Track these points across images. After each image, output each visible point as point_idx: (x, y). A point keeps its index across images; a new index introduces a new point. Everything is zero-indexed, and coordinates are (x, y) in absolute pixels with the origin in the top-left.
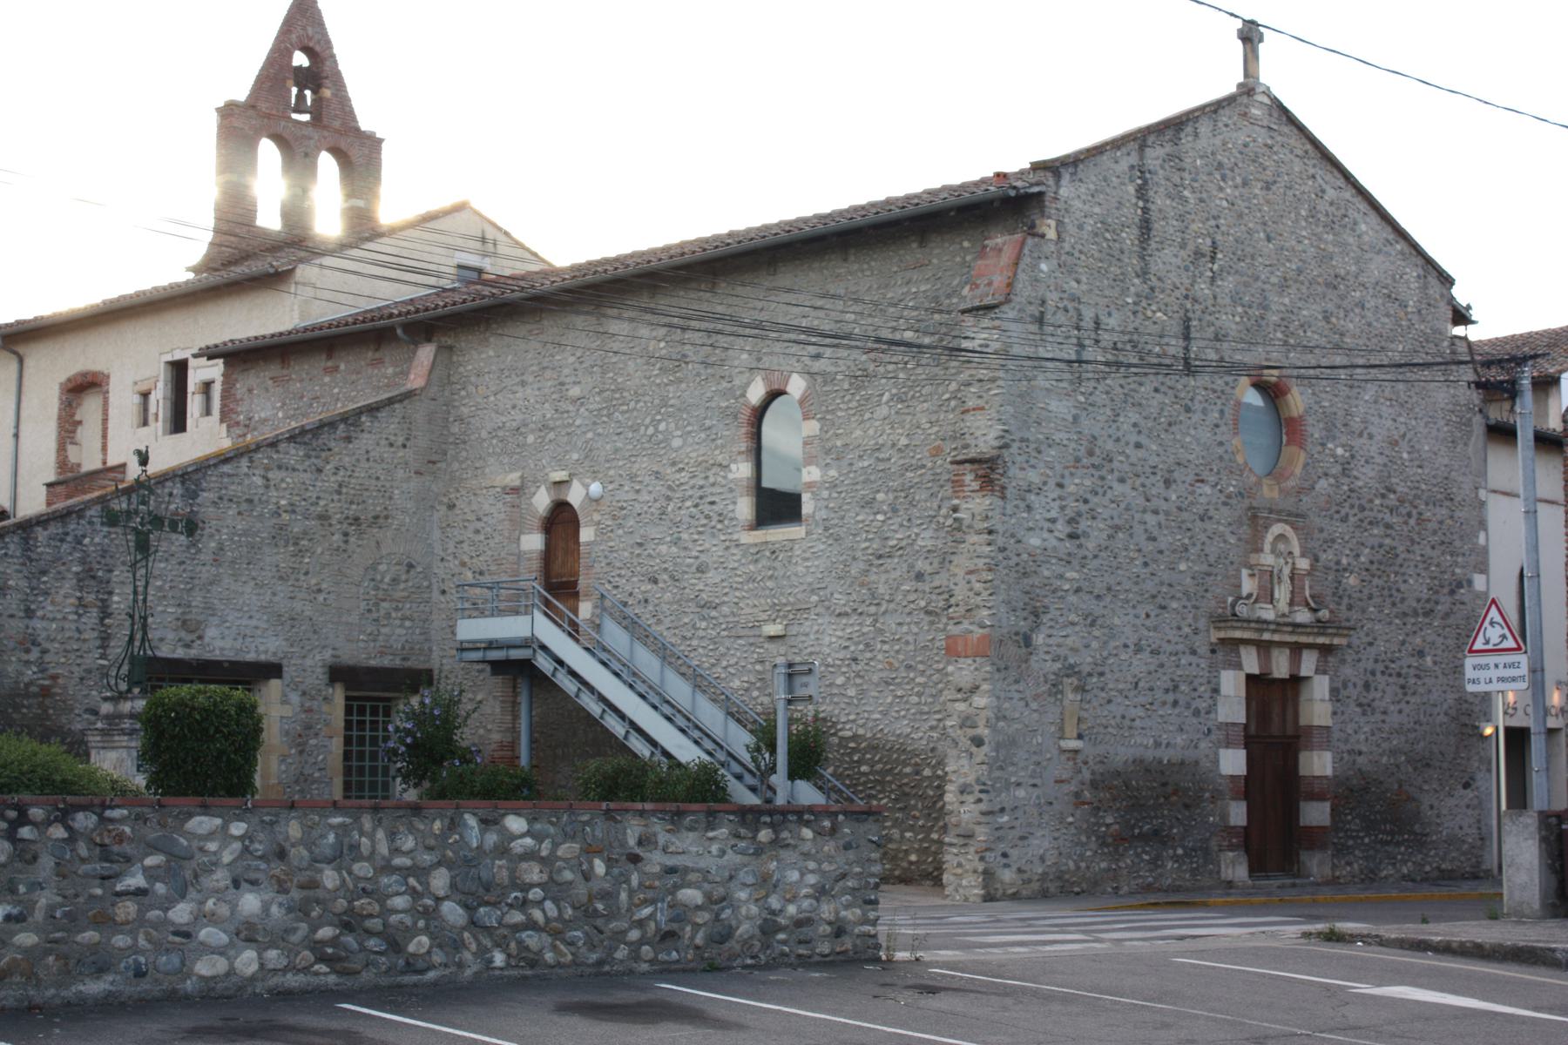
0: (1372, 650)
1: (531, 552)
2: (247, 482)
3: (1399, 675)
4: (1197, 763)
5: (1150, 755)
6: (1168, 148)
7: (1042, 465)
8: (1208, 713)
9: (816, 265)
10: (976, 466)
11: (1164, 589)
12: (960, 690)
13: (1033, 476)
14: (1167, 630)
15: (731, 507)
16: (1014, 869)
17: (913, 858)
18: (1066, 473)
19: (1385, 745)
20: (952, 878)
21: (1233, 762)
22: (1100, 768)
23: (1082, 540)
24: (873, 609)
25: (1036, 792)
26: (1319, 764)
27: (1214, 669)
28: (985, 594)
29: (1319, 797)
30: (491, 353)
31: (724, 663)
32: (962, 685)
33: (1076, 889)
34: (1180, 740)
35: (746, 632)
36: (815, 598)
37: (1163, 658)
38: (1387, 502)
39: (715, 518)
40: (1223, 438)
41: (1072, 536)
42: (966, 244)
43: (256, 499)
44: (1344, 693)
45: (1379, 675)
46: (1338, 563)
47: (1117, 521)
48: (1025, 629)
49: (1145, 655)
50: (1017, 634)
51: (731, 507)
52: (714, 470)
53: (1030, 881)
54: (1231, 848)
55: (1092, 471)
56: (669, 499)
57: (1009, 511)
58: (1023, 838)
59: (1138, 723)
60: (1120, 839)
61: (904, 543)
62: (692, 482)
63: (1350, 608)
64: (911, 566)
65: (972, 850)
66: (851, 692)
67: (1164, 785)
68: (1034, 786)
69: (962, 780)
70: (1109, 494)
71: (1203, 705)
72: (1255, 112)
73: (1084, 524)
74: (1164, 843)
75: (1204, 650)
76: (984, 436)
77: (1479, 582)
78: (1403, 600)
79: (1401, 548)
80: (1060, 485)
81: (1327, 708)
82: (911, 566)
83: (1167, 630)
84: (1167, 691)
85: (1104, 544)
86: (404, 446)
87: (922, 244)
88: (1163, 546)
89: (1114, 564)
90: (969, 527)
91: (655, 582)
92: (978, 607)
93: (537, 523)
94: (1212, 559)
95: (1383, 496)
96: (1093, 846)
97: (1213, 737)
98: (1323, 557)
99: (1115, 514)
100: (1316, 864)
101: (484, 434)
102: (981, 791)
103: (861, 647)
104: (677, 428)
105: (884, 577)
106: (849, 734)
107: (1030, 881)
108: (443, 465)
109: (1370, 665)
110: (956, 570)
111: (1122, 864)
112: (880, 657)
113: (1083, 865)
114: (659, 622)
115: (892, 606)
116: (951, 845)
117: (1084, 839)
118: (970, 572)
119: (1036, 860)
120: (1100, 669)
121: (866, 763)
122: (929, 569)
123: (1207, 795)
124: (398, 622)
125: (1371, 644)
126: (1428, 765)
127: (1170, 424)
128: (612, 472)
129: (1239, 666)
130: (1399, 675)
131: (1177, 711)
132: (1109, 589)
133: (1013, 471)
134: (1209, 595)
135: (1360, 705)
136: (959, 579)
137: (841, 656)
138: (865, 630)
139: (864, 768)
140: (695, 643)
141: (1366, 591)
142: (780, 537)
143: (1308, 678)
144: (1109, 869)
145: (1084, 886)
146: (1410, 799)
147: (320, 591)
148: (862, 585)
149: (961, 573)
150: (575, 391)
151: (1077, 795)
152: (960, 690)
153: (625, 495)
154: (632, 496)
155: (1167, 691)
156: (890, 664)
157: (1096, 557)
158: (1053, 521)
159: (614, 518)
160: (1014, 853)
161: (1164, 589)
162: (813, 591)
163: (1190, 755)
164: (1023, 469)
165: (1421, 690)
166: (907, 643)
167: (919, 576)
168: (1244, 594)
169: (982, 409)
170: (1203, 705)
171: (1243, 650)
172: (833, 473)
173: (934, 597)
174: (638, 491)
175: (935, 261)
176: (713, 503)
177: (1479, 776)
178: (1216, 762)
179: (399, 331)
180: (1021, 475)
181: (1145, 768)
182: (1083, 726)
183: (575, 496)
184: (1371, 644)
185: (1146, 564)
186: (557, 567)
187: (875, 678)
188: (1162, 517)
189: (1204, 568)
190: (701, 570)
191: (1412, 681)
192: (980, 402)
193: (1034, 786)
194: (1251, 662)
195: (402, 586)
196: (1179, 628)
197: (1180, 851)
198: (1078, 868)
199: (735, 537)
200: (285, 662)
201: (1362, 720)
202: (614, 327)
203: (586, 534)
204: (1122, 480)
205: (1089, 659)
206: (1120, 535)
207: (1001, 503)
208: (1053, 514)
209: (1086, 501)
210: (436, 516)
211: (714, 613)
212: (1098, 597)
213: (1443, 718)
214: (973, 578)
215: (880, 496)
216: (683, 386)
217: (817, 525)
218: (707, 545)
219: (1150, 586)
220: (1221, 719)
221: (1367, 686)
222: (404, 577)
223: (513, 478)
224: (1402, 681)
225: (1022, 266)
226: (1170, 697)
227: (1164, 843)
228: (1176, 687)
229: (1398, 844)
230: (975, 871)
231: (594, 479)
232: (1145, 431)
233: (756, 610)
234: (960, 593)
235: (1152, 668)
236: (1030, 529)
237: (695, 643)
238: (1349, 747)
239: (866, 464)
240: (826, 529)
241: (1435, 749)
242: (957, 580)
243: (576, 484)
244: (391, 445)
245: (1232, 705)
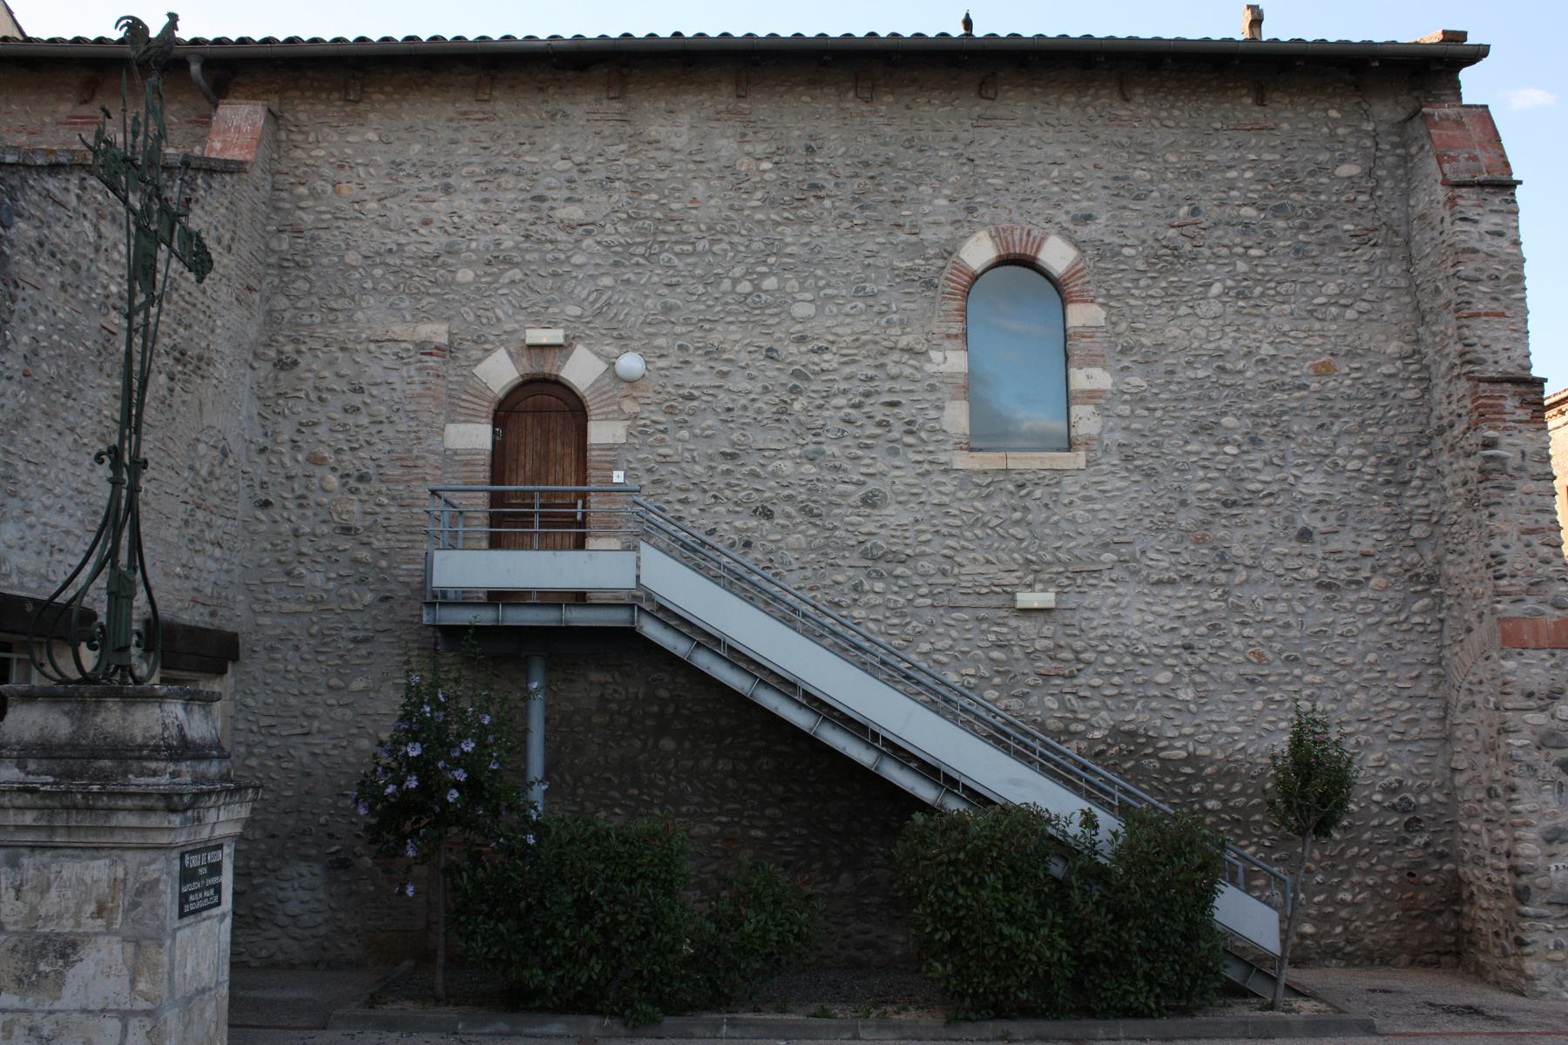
9: (1070, 99)
10: (1523, 389)
12: (1530, 695)
15: (932, 414)
24: (1222, 577)
30: (372, 136)
32: (1534, 688)
35: (970, 601)
36: (1108, 557)
42: (1334, 114)
45: (1462, 692)
51: (932, 414)
52: (896, 356)
56: (795, 390)
61: (1275, 488)
62: (847, 370)
64: (1289, 521)
66: (1186, 694)
69: (1546, 824)
82: (1289, 521)
87: (1260, 101)
90: (1520, 469)
91: (768, 515)
93: (488, 409)
103: (1202, 630)
104: (803, 289)
105: (1239, 534)
112: (1238, 644)
115: (1257, 574)
116: (1539, 917)
121: (1215, 795)
122: (1321, 526)
136: (1512, 538)
137: (1164, 640)
138: (1208, 605)
142: (1036, 465)
148: (1200, 541)
152: (1530, 695)
153: (698, 375)
154: (709, 380)
159: (671, 411)
162: (1105, 546)
166: (1287, 626)
167: (1305, 535)
169: (1502, 315)
172: (1136, 380)
173: (1332, 565)
174: (723, 374)
179: (195, 68)
187: (1231, 675)
199: (943, 458)
202: (656, 129)
203: (601, 433)
211: (900, 570)
214: (1535, 540)
215: (1228, 421)
216: (815, 229)
217: (1106, 451)
218: (880, 467)
231: (625, 349)
233: (992, 569)
239: (1201, 374)
240: (1128, 459)
242: (1508, 540)
243: (581, 353)
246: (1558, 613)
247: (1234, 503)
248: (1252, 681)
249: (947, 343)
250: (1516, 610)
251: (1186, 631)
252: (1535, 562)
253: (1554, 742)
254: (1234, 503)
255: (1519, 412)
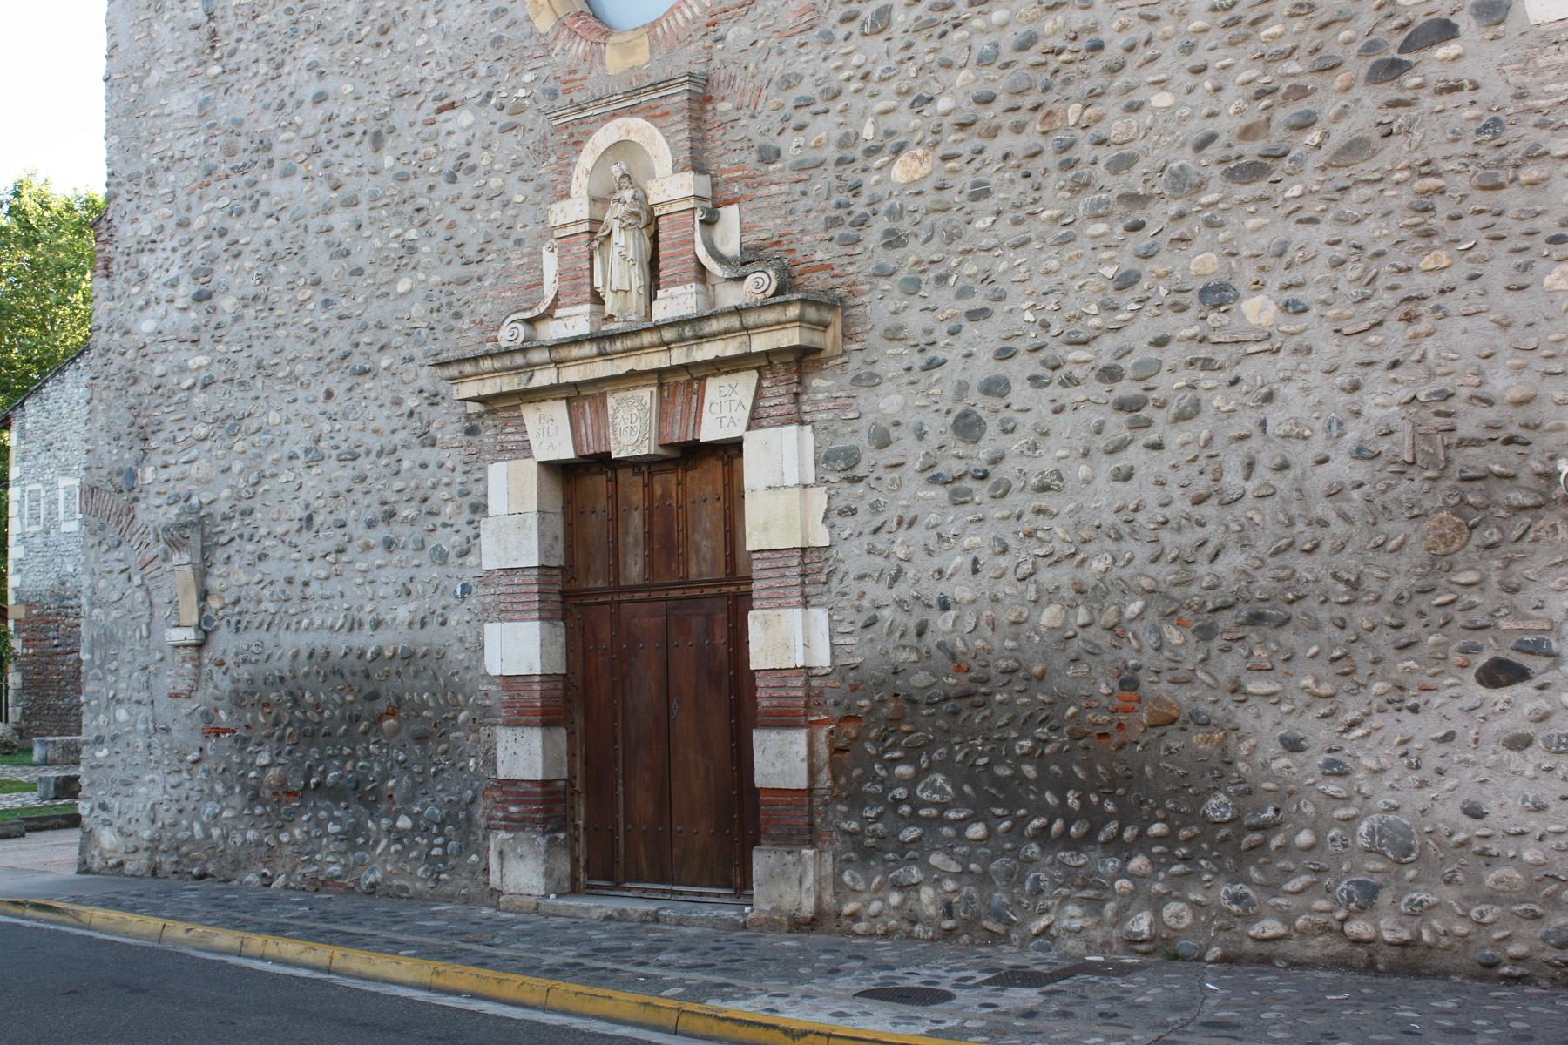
5: (339, 643)
8: (463, 554)
19: (1063, 575)
21: (519, 648)
22: (244, 672)
27: (475, 464)
29: (783, 719)
37: (364, 464)
48: (131, 464)
49: (330, 466)
54: (512, 824)
55: (235, 179)
58: (126, 784)
59: (314, 588)
60: (283, 792)
67: (373, 696)
70: (264, 206)
71: (449, 541)
74: (371, 806)
75: (448, 428)
84: (370, 525)
85: (251, 292)
89: (272, 320)
94: (471, 251)
96: (237, 801)
97: (473, 601)
99: (272, 234)
100: (786, 881)
111: (284, 838)
117: (219, 789)
120: (245, 505)
125: (976, 315)
127: (384, 31)
129: (526, 449)
134: (465, 323)
144: (259, 844)
151: (208, 716)
155: (370, 525)
163: (432, 636)
170: (449, 541)
171: (529, 414)
181: (328, 667)
184: (976, 315)
189: (457, 270)
194: (551, 434)
196: (398, 402)
197: (404, 822)
207: (105, 283)
209: (223, 233)
219: (339, 341)
220: (487, 564)
227: (371, 806)
235: (341, 487)
238: (903, 589)
245: (514, 525)
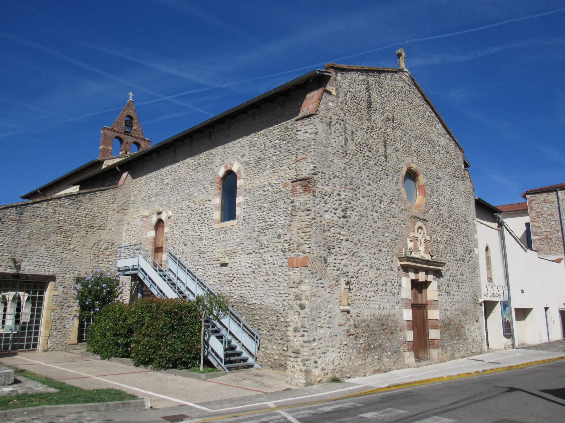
0: (449, 272)
1: (150, 237)
2: (46, 210)
3: (457, 282)
4: (394, 315)
5: (377, 312)
6: (377, 78)
7: (331, 184)
10: (302, 182)
11: (380, 243)
13: (328, 189)
14: (382, 260)
16: (320, 368)
17: (276, 357)
18: (341, 190)
20: (290, 373)
23: (348, 219)
25: (330, 330)
26: (433, 314)
27: (399, 276)
28: (306, 238)
29: (436, 327)
31: (207, 275)
33: (348, 376)
34: (388, 305)
36: (240, 248)
37: (381, 271)
38: (450, 220)
39: (206, 220)
40: (399, 188)
41: (344, 217)
43: (49, 216)
44: (441, 288)
46: (437, 240)
47: (362, 213)
49: (374, 270)
50: (321, 257)
53: (327, 374)
54: (409, 350)
55: (351, 191)
56: (192, 214)
57: (316, 203)
58: (324, 353)
63: (442, 256)
65: (299, 360)
66: (252, 285)
68: (329, 327)
69: (295, 325)
71: (395, 291)
72: (404, 77)
73: (349, 213)
76: (306, 171)
77: (476, 250)
78: (456, 255)
79: (455, 237)
80: (339, 195)
81: (437, 293)
83: (382, 260)
86: (113, 203)
88: (380, 226)
90: (299, 209)
91: (186, 245)
92: (302, 244)
94: (397, 233)
95: (449, 218)
97: (400, 304)
98: (433, 237)
100: (434, 353)
101: (140, 199)
102: (304, 331)
106: (252, 303)
107: (327, 374)
108: (128, 211)
109: (448, 278)
110: (293, 228)
113: (351, 363)
114: (187, 260)
117: (351, 351)
118: (299, 229)
119: (330, 363)
122: (283, 233)
123: (398, 329)
124: (106, 262)
125: (448, 270)
126: (466, 314)
128: (175, 207)
129: (408, 276)
130: (457, 282)
131: (386, 294)
132: (359, 241)
133: (319, 185)
135: (446, 292)
139: (257, 317)
140: (198, 267)
141: (446, 251)
143: (430, 282)
145: (352, 374)
146: (462, 327)
147: (74, 251)
149: (295, 229)
150: (166, 181)
151: (348, 331)
156: (267, 273)
157: (354, 227)
158: (336, 209)
160: (320, 361)
161: (380, 243)
163: (392, 312)
164: (323, 185)
165: (463, 287)
168: (409, 248)
169: (305, 158)
175: (287, 113)
176: (205, 215)
177: (480, 318)
178: (401, 315)
180: (321, 187)
182: (350, 300)
183: (164, 217)
185: (373, 232)
186: (157, 243)
188: (379, 214)
189: (394, 236)
190: (201, 239)
191: (461, 284)
192: (304, 156)
193: (329, 327)
195: (109, 250)
196: (387, 260)
197: (389, 353)
198: (349, 365)
200: (57, 275)
201: (447, 298)
204: (363, 197)
205: (352, 270)
206: (363, 219)
208: (336, 206)
210: (124, 227)
211: (205, 256)
212: (355, 244)
213: (469, 297)
214: (300, 231)
219: (375, 241)
221: (448, 285)
222: (110, 247)
223: (147, 213)
224: (458, 284)
225: (322, 101)
226: (384, 288)
228: (386, 284)
229: (460, 344)
230: (301, 371)
232: (372, 179)
234: (295, 239)
236: (326, 211)
237: (198, 267)
241: (468, 308)
244: (108, 203)
246: (304, 255)
247: (265, 229)
248: (266, 281)
249: (215, 197)
250: (293, 255)
251: (253, 267)
252: (299, 238)
253: (298, 298)
254: (265, 229)
255: (301, 190)
